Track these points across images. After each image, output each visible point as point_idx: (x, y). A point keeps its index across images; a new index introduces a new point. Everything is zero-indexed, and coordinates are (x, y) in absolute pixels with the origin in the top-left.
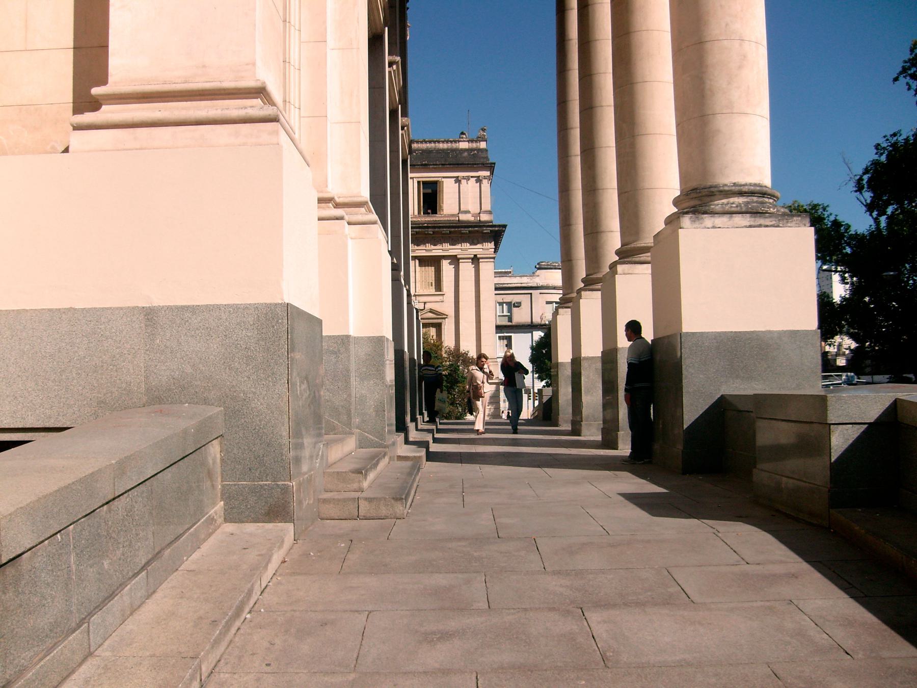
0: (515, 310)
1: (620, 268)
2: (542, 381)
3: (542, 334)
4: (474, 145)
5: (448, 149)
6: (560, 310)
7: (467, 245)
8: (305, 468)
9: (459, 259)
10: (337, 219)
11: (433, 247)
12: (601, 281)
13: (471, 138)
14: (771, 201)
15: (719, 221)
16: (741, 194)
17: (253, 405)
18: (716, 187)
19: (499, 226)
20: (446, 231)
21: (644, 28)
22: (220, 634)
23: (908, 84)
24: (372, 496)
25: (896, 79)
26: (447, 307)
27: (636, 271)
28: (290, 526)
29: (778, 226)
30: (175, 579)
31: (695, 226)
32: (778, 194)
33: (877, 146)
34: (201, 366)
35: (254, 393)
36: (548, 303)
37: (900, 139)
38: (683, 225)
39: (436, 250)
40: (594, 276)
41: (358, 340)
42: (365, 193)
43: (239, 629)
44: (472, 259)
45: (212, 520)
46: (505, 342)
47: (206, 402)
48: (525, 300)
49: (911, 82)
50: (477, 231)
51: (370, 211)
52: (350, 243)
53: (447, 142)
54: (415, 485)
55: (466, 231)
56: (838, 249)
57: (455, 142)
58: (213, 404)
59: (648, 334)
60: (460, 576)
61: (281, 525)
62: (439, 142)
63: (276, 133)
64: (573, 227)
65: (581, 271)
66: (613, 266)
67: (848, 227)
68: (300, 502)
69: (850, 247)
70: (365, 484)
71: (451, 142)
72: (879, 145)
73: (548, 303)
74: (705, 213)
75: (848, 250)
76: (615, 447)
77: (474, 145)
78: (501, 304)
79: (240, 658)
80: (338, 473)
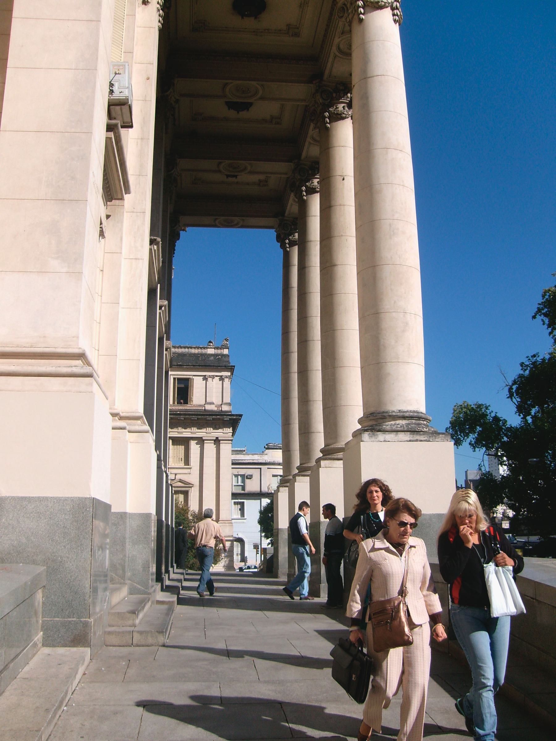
0: (247, 481)
1: (323, 463)
2: (268, 538)
3: (269, 501)
4: (219, 351)
5: (198, 354)
6: (281, 489)
7: (210, 430)
8: (98, 609)
9: (204, 440)
10: (121, 429)
11: (184, 430)
12: (309, 469)
13: (216, 346)
14: (425, 422)
15: (388, 436)
16: (404, 418)
17: (67, 566)
18: (387, 412)
19: (237, 415)
20: (195, 418)
21: (343, 292)
22: (52, 717)
23: (543, 320)
24: (143, 630)
25: (534, 317)
26: (194, 478)
27: (335, 466)
28: (88, 650)
29: (429, 441)
30: (15, 684)
31: (372, 440)
32: (431, 418)
33: (522, 364)
34: (32, 538)
35: (68, 558)
36: (274, 476)
37: (538, 359)
38: (363, 439)
39: (186, 433)
40: (306, 465)
41: (132, 515)
42: (140, 410)
43: (60, 716)
44: (215, 440)
45: (35, 645)
46: (239, 506)
47: (34, 562)
48: (255, 473)
49: (544, 318)
50: (219, 419)
51: (145, 424)
52: (129, 444)
53: (198, 348)
54: (171, 623)
55: (210, 418)
56: (498, 438)
57: (204, 348)
58: (39, 564)
59: (340, 514)
60: (203, 684)
61: (82, 649)
62: (191, 348)
63: (91, 384)
64: (292, 426)
65: (297, 462)
66: (318, 461)
67: (505, 421)
68: (95, 634)
69: (507, 437)
70: (137, 621)
71: (201, 348)
72: (523, 363)
73: (274, 476)
74: (379, 431)
75: (505, 439)
76: (318, 596)
77: (219, 351)
78: (236, 476)
79: (63, 733)
80: (118, 613)
